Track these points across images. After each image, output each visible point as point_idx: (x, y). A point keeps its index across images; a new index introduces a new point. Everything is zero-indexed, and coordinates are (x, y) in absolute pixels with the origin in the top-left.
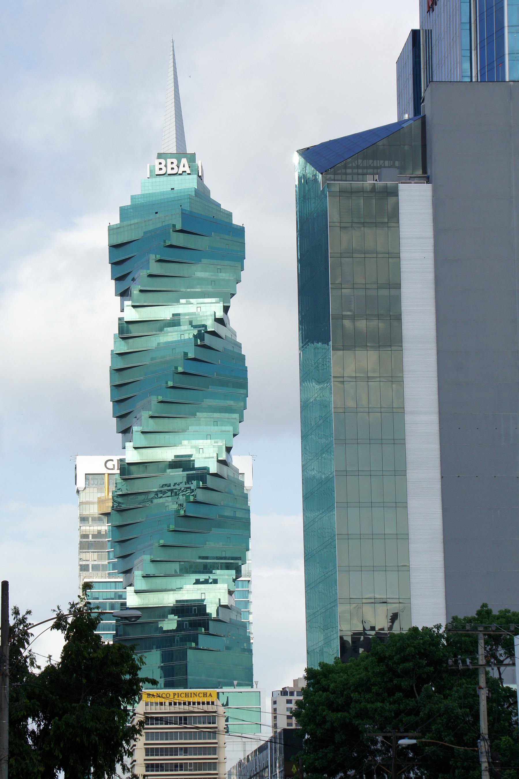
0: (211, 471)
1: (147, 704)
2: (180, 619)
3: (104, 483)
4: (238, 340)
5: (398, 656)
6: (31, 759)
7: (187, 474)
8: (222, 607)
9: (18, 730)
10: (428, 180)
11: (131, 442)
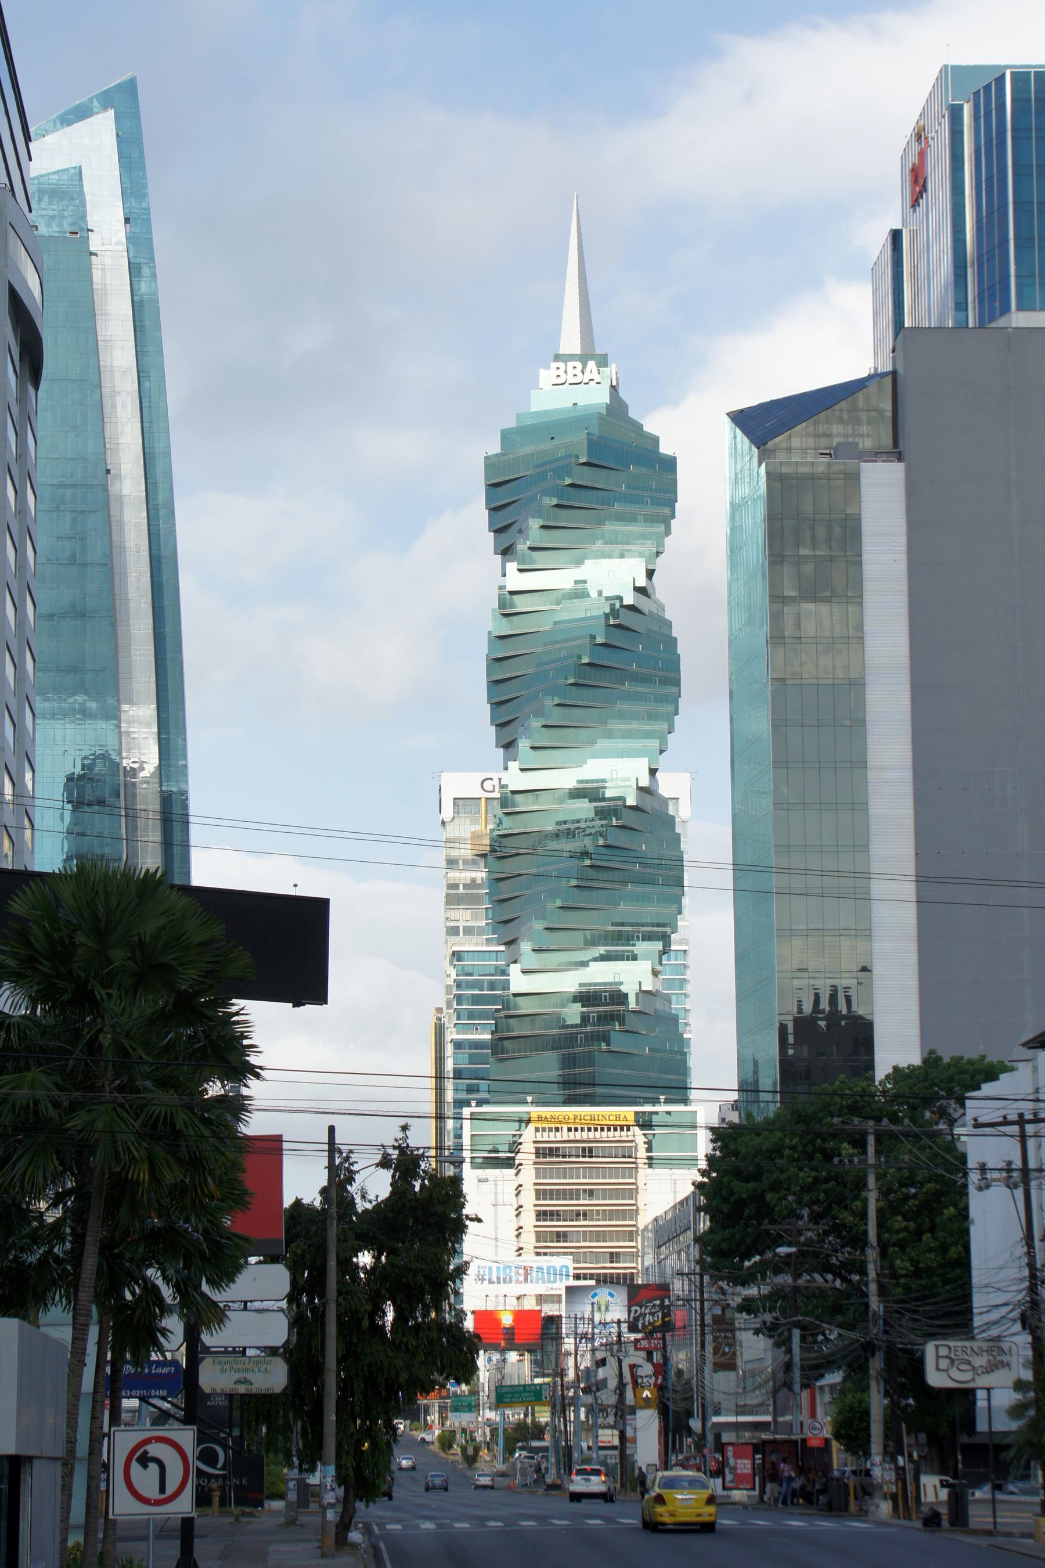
1: (537, 1130)
2: (584, 1009)
3: (479, 812)
6: (359, 1298)
8: (643, 994)
10: (900, 459)
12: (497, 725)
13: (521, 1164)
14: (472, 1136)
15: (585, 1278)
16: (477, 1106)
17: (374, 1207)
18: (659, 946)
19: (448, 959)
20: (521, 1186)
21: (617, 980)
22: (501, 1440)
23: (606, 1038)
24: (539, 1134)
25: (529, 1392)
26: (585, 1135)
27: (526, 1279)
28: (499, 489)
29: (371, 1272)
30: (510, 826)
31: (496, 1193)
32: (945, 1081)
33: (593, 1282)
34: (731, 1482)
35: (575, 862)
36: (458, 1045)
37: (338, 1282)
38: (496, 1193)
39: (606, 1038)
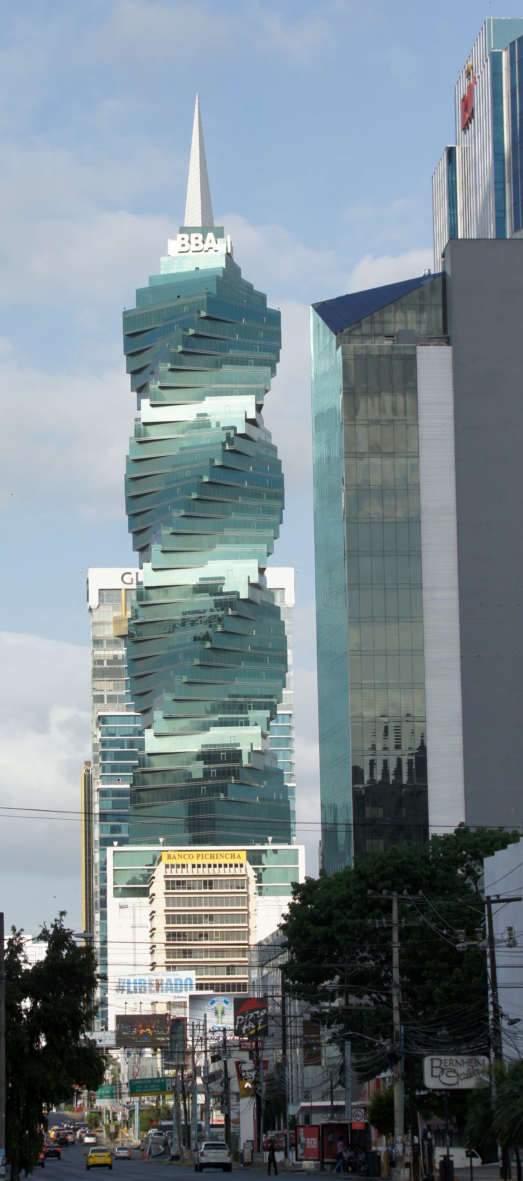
0: (242, 596)
1: (167, 866)
2: (206, 766)
3: (120, 601)
4: (274, 442)
5: (378, 875)
7: (214, 600)
8: (253, 753)
9: (13, 1011)
10: (448, 343)
11: (149, 562)
12: (133, 533)
13: (154, 895)
14: (114, 870)
15: (207, 989)
16: (119, 845)
17: (34, 968)
18: (267, 713)
19: (95, 722)
20: (154, 912)
21: (233, 742)
22: (137, 1119)
23: (223, 789)
24: (169, 870)
25: (156, 1084)
26: (206, 871)
27: (158, 990)
28: (135, 338)
29: (31, 1013)
30: (145, 616)
31: (134, 917)
32: (477, 843)
33: (211, 992)
34: (301, 1155)
35: (198, 645)
36: (103, 793)
37: (6, 1022)
38: (134, 917)
39: (223, 789)
